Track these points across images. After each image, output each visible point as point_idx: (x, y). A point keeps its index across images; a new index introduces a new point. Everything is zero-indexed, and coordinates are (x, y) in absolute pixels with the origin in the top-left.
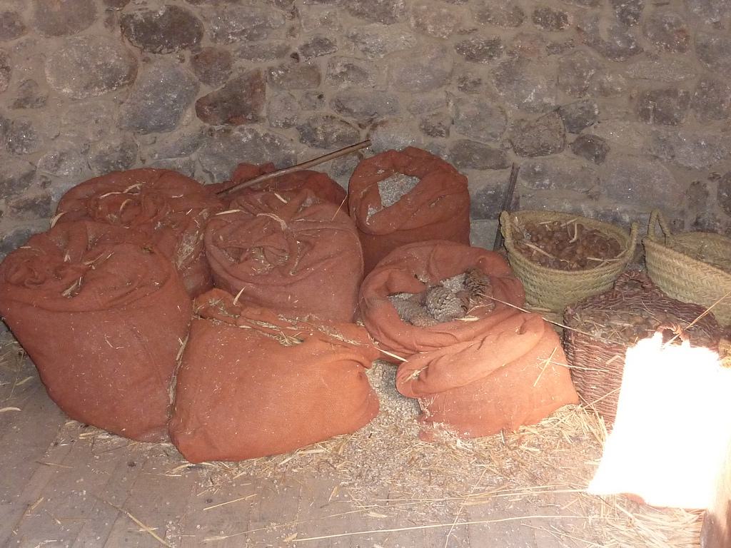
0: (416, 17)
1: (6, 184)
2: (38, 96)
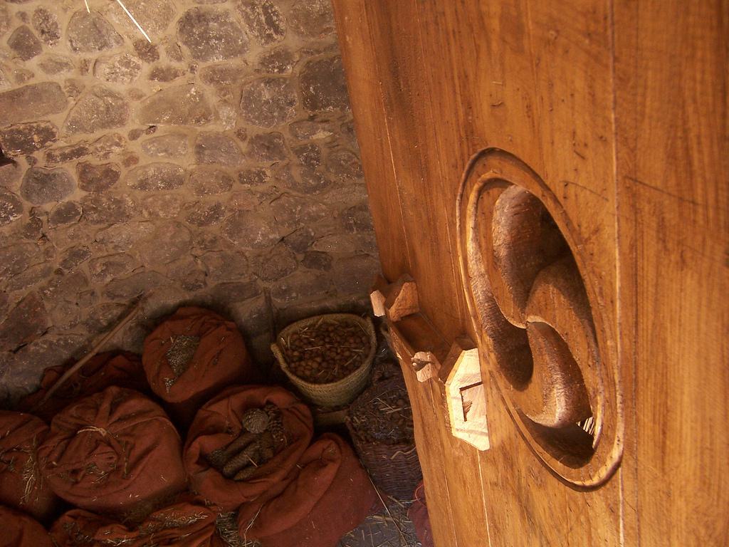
0: (146, 209)
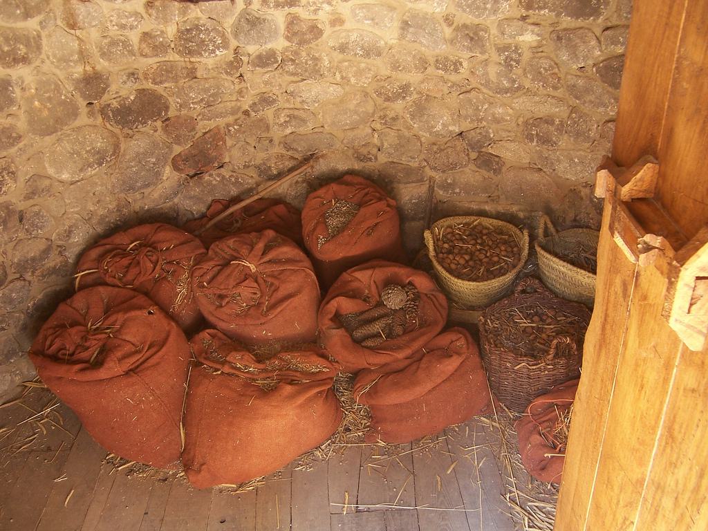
0: (340, 72)
1: (29, 262)
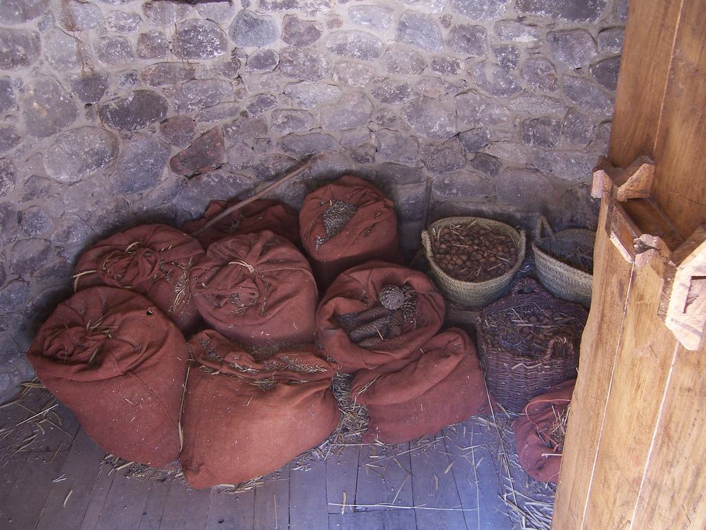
2: (41, 188)
